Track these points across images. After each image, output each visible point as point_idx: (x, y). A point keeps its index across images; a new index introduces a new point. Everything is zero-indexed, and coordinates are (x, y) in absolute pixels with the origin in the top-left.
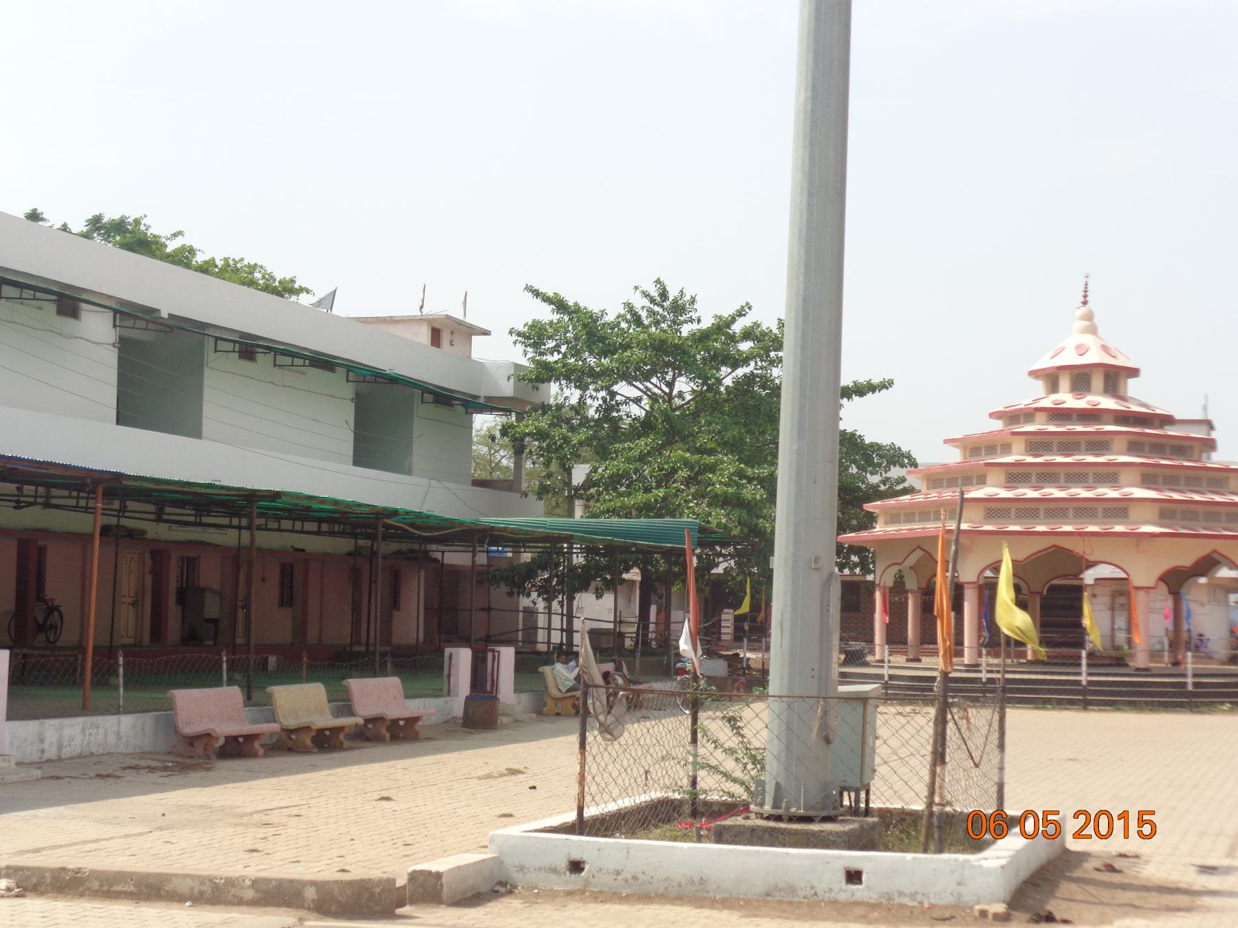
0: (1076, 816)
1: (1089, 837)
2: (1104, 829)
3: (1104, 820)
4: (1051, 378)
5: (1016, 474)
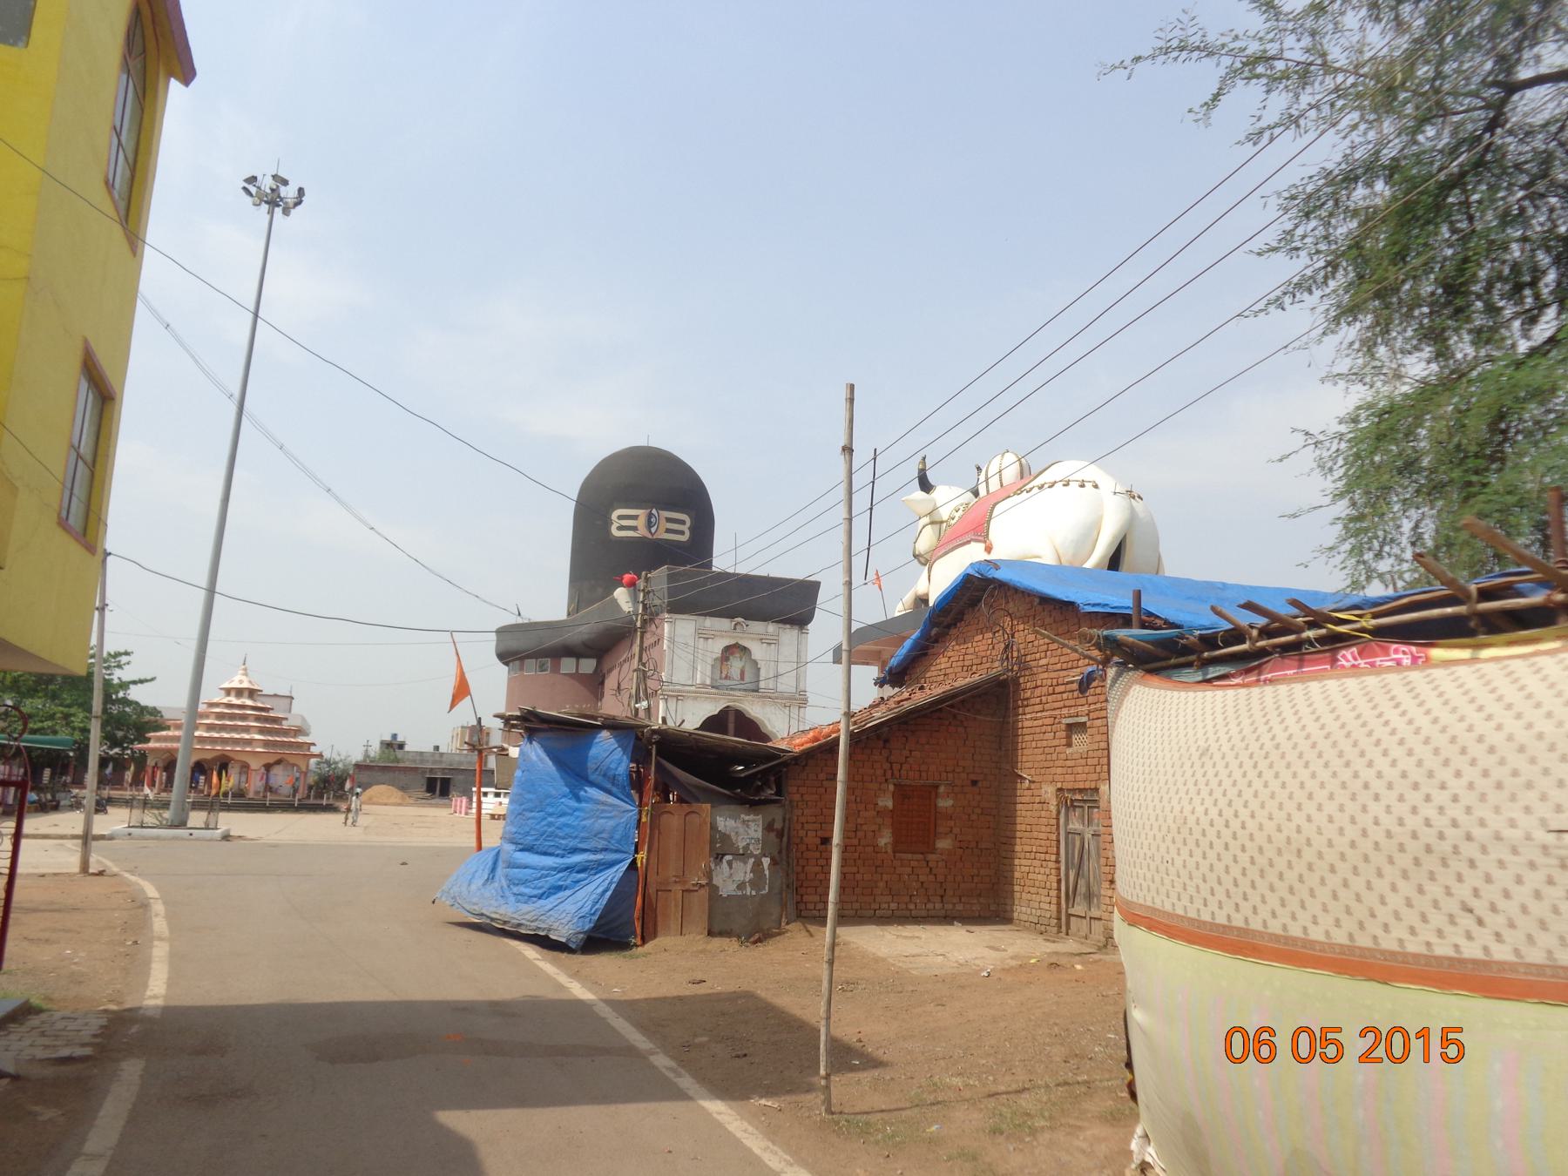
0: (1363, 1033)
1: (1380, 1060)
2: (1398, 1052)
3: (1398, 1039)
4: (228, 691)
5: (210, 727)
